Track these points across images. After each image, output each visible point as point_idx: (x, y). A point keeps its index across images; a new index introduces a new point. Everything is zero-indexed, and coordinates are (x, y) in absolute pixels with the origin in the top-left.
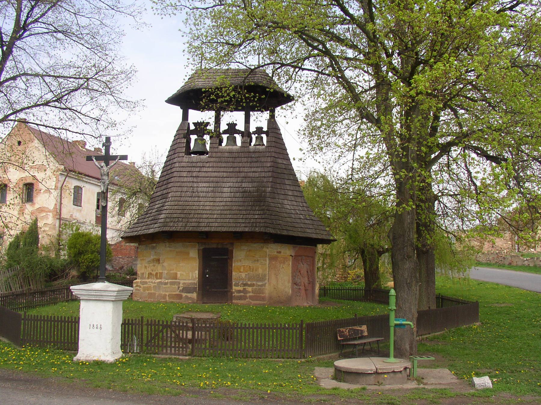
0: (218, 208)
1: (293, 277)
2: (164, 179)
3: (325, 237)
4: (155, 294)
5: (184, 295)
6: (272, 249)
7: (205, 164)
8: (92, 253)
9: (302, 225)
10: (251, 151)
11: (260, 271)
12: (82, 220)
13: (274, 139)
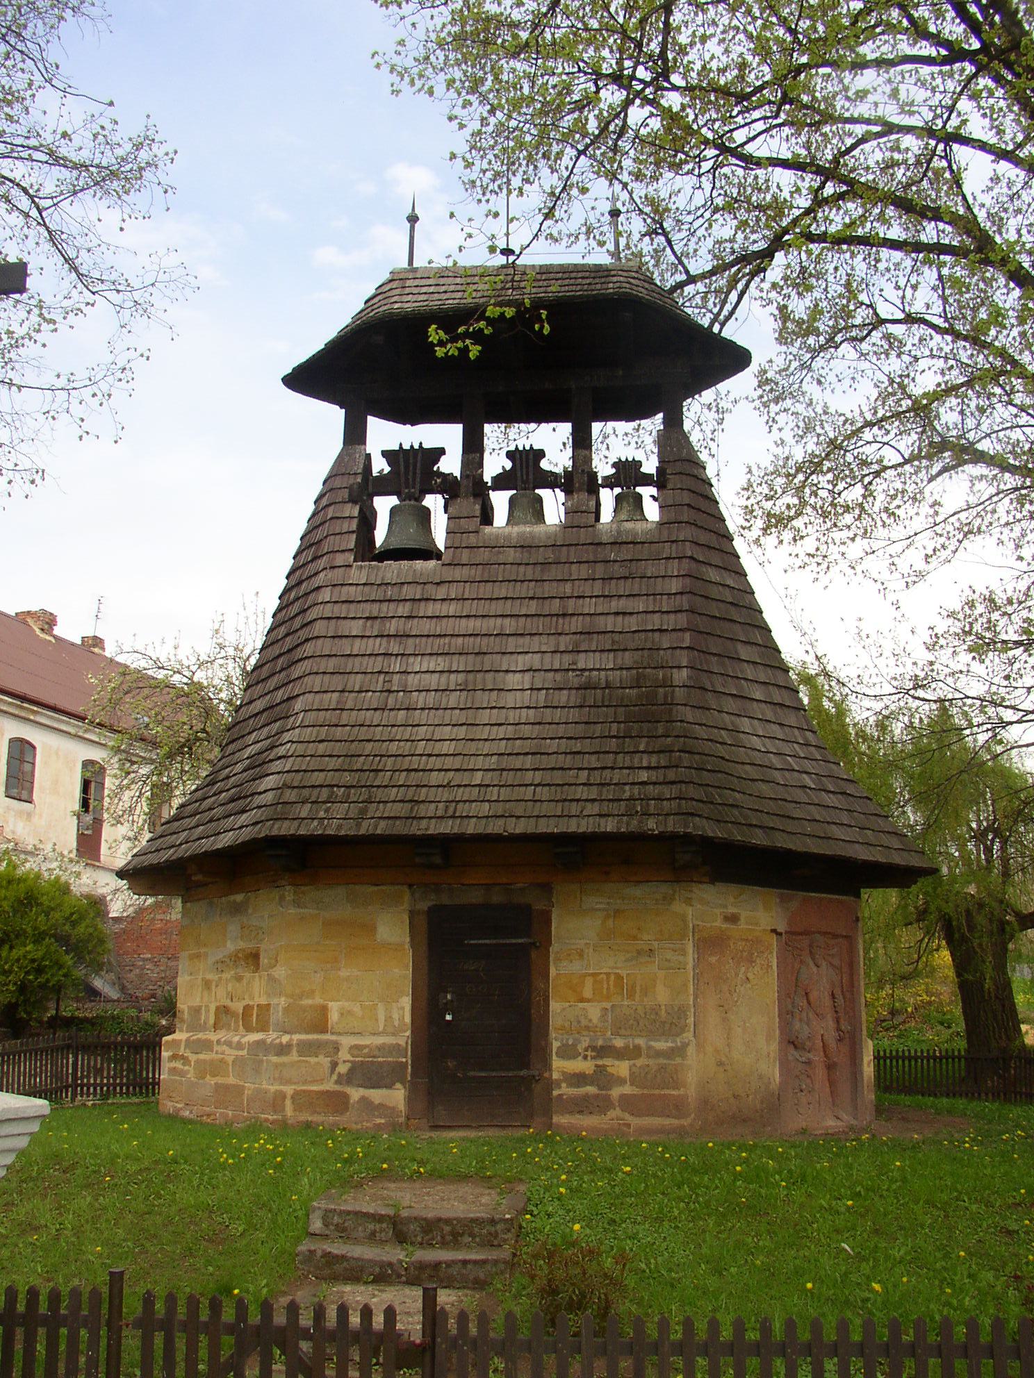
0: (486, 748)
1: (786, 1015)
2: (276, 650)
3: (898, 859)
4: (239, 1090)
5: (355, 1094)
6: (709, 905)
7: (431, 591)
8: (39, 938)
9: (816, 813)
10: (605, 539)
11: (662, 995)
12: (29, 842)
13: (686, 498)
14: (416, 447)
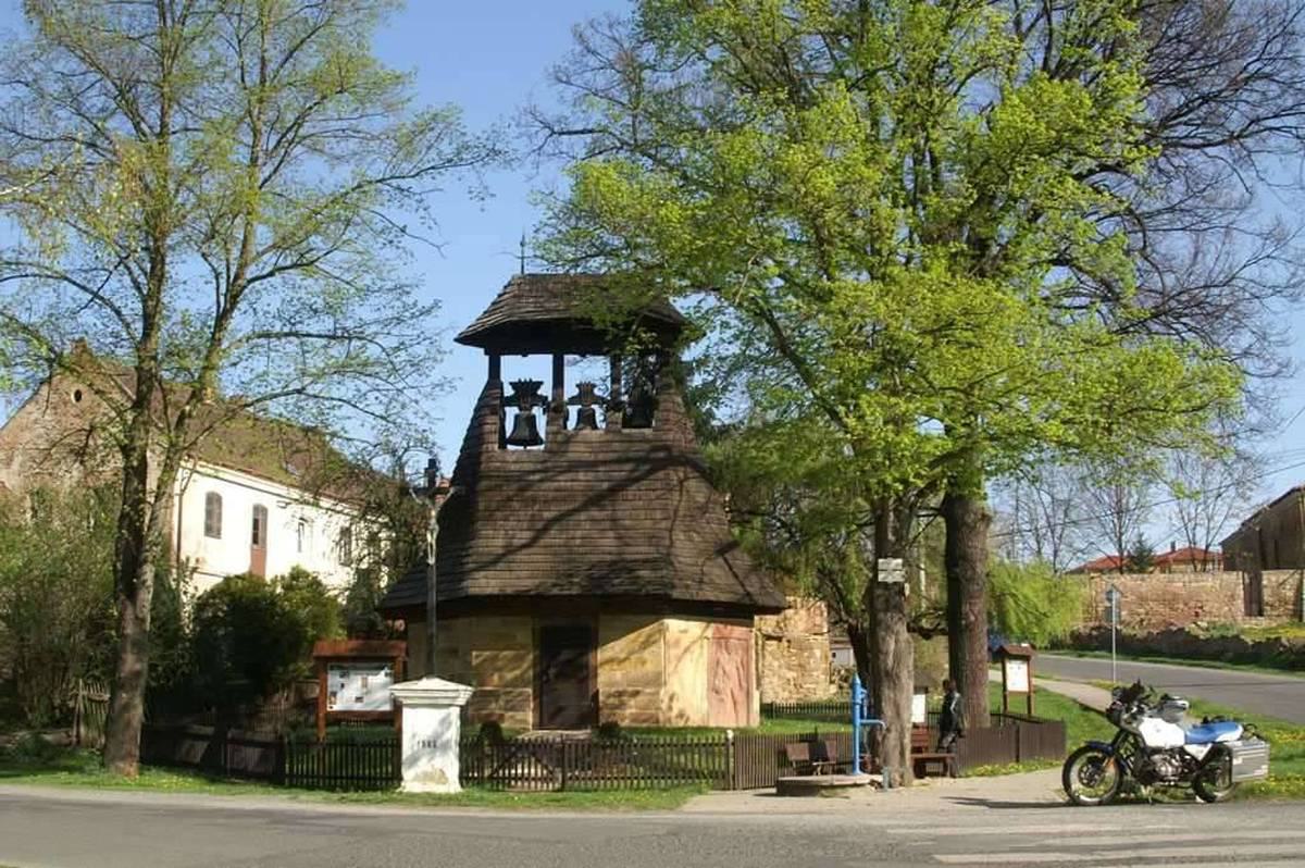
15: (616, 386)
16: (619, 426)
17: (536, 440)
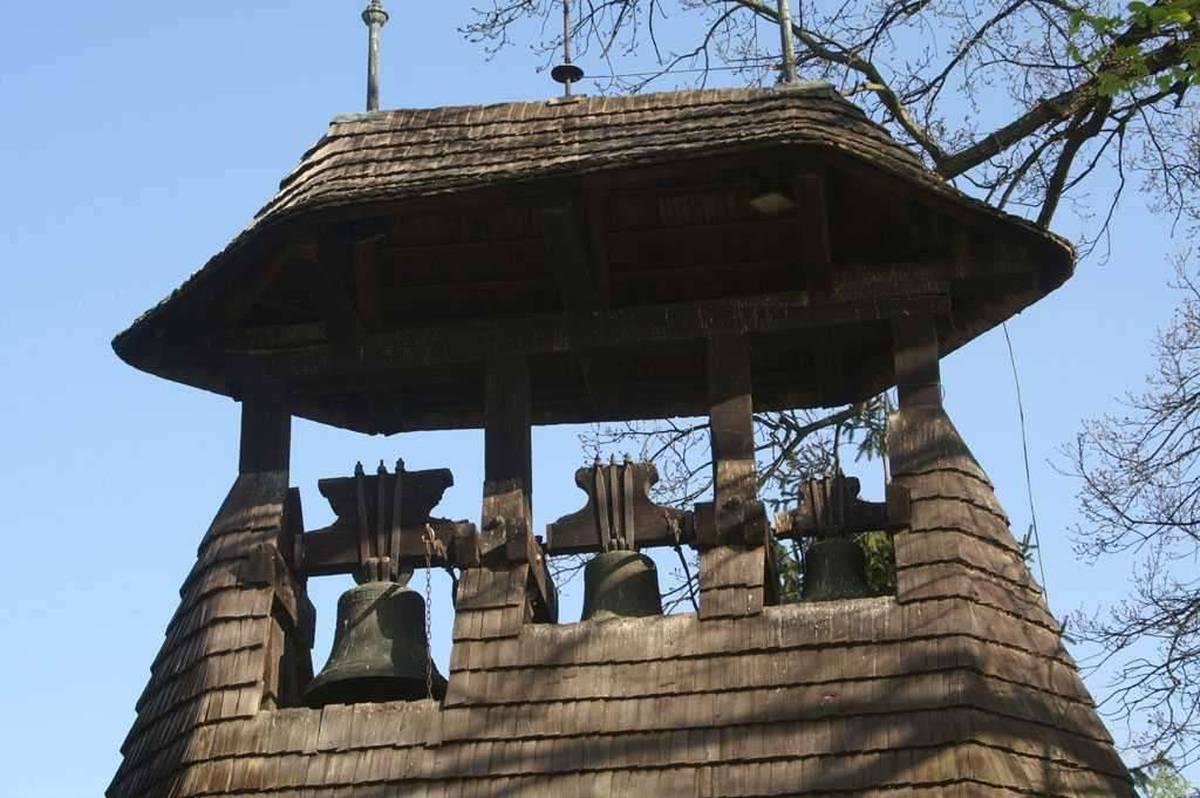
14: (391, 470)
15: (732, 469)
16: (755, 598)
17: (410, 679)
